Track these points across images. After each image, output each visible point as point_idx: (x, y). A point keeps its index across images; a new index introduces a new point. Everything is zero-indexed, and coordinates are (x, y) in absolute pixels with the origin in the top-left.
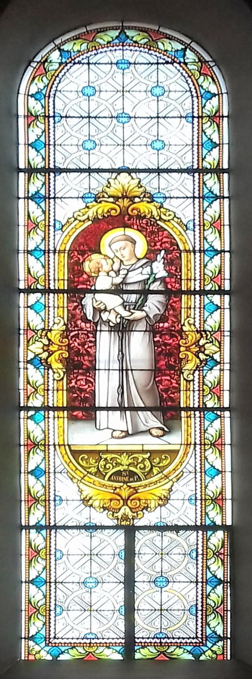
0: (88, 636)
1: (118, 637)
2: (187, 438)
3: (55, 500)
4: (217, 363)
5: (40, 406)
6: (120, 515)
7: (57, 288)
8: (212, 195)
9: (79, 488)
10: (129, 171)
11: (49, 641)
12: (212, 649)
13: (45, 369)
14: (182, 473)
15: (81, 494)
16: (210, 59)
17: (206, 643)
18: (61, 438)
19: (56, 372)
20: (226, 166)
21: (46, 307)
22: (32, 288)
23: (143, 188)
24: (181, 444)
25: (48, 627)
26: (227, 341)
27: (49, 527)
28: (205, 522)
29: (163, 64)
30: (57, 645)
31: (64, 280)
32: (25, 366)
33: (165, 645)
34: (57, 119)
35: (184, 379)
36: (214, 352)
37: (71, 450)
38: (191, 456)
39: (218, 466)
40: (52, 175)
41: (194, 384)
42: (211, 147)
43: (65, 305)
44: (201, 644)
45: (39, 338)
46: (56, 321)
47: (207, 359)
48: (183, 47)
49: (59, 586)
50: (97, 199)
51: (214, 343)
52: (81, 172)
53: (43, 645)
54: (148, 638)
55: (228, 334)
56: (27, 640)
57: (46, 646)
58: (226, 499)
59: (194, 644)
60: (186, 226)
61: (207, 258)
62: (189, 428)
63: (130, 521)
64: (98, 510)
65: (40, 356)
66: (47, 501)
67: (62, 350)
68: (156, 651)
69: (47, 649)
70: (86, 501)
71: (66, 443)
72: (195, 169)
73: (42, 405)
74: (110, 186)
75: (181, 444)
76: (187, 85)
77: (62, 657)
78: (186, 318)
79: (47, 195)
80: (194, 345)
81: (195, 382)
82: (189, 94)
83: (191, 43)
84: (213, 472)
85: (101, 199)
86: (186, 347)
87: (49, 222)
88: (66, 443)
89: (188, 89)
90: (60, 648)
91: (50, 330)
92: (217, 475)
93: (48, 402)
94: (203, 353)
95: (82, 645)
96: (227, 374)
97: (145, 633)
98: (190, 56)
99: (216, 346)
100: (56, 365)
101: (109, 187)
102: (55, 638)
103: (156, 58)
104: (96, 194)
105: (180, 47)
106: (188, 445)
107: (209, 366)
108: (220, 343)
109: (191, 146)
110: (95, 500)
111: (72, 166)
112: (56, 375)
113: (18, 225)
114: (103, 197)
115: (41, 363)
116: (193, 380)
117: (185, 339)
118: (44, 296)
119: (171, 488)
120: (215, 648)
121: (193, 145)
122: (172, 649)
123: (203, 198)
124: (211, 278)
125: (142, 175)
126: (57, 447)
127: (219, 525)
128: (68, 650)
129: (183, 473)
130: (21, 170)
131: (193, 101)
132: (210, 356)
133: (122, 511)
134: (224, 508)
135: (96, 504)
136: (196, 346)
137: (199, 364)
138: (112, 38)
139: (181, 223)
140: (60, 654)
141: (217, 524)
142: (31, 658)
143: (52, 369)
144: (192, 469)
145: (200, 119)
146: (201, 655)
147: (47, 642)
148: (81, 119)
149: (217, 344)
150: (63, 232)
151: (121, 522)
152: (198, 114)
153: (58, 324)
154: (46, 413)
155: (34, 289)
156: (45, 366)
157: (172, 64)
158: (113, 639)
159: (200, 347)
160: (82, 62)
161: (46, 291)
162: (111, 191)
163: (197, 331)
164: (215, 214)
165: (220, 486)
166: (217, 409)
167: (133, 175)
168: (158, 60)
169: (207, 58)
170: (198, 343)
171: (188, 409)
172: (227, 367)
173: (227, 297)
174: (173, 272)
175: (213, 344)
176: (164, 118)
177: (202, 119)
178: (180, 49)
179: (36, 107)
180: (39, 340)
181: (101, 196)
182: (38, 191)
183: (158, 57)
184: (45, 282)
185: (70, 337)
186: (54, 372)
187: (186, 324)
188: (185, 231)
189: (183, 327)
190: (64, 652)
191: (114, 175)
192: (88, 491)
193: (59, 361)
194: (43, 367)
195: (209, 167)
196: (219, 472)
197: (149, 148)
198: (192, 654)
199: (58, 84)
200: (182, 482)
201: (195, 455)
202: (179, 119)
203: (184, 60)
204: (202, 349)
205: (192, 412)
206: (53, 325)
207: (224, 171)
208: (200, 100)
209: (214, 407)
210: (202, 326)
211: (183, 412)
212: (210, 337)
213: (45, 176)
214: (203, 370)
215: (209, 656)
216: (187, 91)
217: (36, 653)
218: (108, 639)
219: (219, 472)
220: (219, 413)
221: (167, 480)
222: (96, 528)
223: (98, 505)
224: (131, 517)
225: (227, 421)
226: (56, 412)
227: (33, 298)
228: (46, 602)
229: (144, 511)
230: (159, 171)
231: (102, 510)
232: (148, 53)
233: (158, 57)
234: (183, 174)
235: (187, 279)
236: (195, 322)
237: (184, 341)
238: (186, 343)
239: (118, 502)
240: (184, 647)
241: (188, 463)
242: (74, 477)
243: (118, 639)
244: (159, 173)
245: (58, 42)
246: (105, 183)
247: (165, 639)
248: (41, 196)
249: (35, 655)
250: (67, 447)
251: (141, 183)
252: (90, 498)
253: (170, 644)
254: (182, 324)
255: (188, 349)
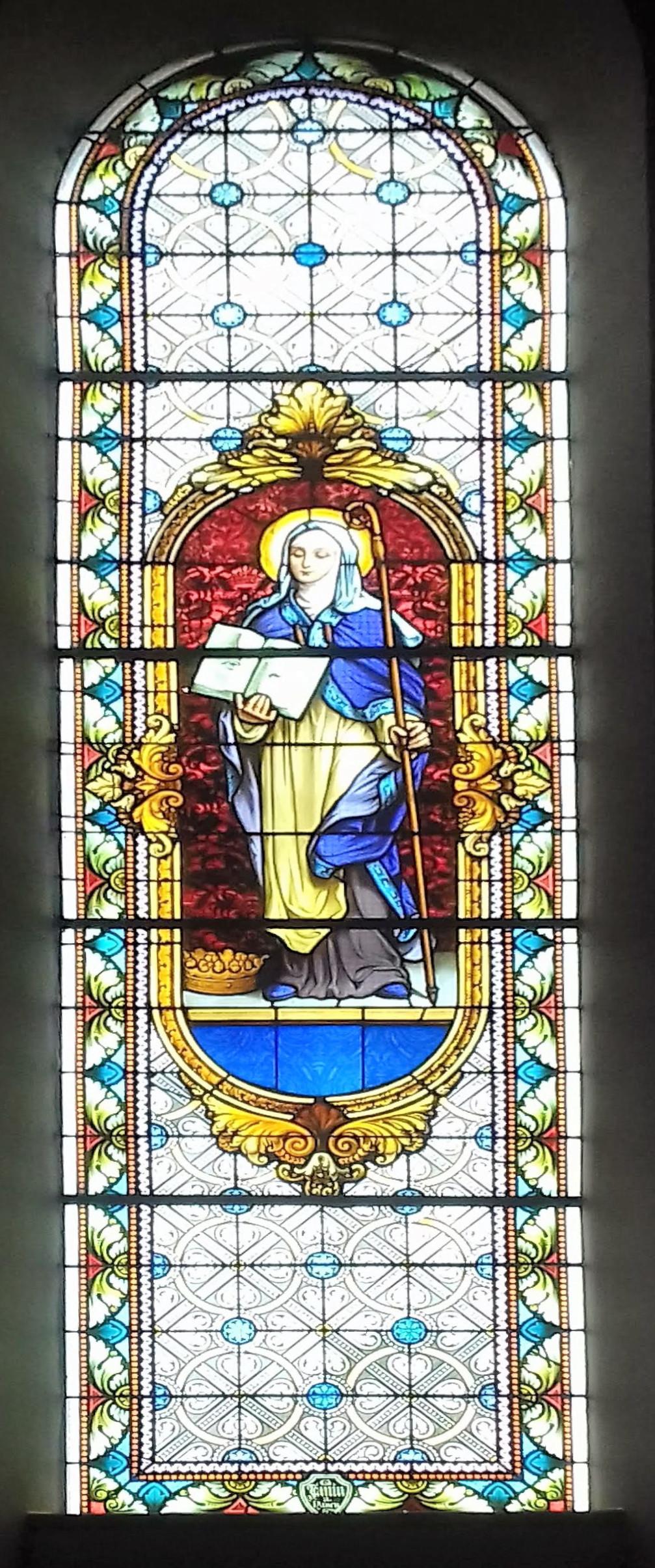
0: (233, 1457)
1: (309, 1459)
2: (472, 992)
3: (149, 1135)
4: (546, 817)
5: (116, 917)
6: (308, 1170)
7: (148, 645)
8: (525, 435)
9: (208, 1111)
10: (324, 377)
11: (138, 1468)
12: (537, 1486)
13: (126, 833)
14: (458, 1075)
15: (214, 1122)
16: (523, 123)
17: (522, 1473)
18: (166, 992)
19: (154, 839)
20: (558, 364)
21: (127, 691)
22: (89, 645)
23: (357, 417)
24: (457, 1007)
25: (136, 1435)
26: (567, 767)
27: (135, 1199)
28: (516, 1191)
29: (406, 130)
30: (159, 1477)
31: (165, 627)
32: (80, 826)
33: (248, 1479)
34: (158, 1270)
35: (468, 854)
36: (536, 791)
37: (188, 1021)
38: (482, 1035)
39: (552, 1316)
40: (138, 386)
41: (490, 867)
42: (521, 322)
43: (174, 687)
44: (509, 1477)
45: (112, 765)
46: (152, 721)
47: (521, 807)
48: (454, 92)
49: (162, 1339)
50: (247, 442)
51: (536, 770)
52: (377, 382)
53: (124, 1477)
54: (381, 1462)
55: (64, 748)
56: (85, 1467)
57: (131, 1480)
58: (77, 1137)
59: (493, 1477)
60: (462, 504)
61: (512, 577)
62: (477, 968)
63: (332, 1187)
64: (254, 1159)
65: (116, 805)
66: (513, 1136)
67: (167, 789)
68: (400, 1494)
69: (134, 1487)
70: (223, 1139)
71: (178, 1004)
72: (492, 657)
73: (120, 914)
74: (279, 412)
75: (457, 1007)
76: (460, 177)
77: (172, 1507)
78: (466, 714)
79: (127, 433)
80: (489, 777)
81: (492, 862)
82: (467, 198)
83: (472, 84)
84: (535, 1072)
85: (256, 442)
86: (470, 781)
87: (130, 493)
88: (178, 1004)
89: (464, 188)
90: (167, 1484)
91: (139, 746)
92: (546, 1078)
93: (136, 908)
94: (512, 794)
95: (391, 1476)
96: (569, 842)
97: (372, 1450)
98: (470, 115)
99: (540, 777)
100: (153, 823)
101: (275, 415)
102: (152, 1459)
103: (386, 116)
104: (243, 429)
105: (446, 91)
106: (476, 1008)
107: (528, 822)
108: (550, 771)
109: (475, 317)
110: (247, 1137)
111: (187, 367)
112: (154, 848)
113: (578, 943)
114: (262, 436)
115: (118, 819)
116: (489, 857)
117: (465, 763)
118: (120, 666)
119: (434, 1109)
120: (544, 1485)
121: (479, 313)
122: (263, 1488)
123: (506, 561)
124: (522, 621)
125: (353, 388)
126: (156, 1013)
127: (550, 1196)
128: (185, 1488)
129: (463, 1073)
130: (66, 377)
131: (478, 215)
132: (527, 800)
133: (314, 1161)
134: (557, 900)
135: (251, 1145)
136: (494, 778)
137: (501, 820)
138: (285, 68)
139: (449, 497)
140: (166, 1499)
141: (546, 1193)
142: (98, 1508)
143: (144, 833)
144: (485, 1066)
145: (497, 257)
146: (509, 1503)
147: (135, 1471)
148: (209, 257)
149: (543, 772)
150: (166, 516)
151: (312, 1188)
152: (492, 244)
153: (157, 729)
154: (131, 934)
155: (532, 646)
156: (126, 826)
157: (430, 132)
158: (467, 1463)
159: (503, 781)
160: (214, 127)
161: (126, 655)
162: (282, 424)
163: (494, 743)
164: (533, 477)
165: (544, 720)
166: (545, 923)
167: (336, 387)
168: (391, 122)
169: (516, 120)
170: (136, 798)
171: (474, 923)
172: (570, 824)
173: (565, 663)
174: (430, 606)
175: (534, 774)
176: (243, 254)
177: (501, 257)
178: (446, 95)
179: (101, 228)
180: (113, 768)
181: (257, 435)
182: (105, 425)
183: (391, 115)
184: (120, 631)
185: (184, 760)
186: (149, 841)
187: (467, 728)
188: (459, 516)
189: (459, 735)
190: (177, 1493)
191: (289, 386)
192: (227, 1116)
193: (160, 815)
194: (122, 829)
195: (518, 368)
196: (550, 1072)
197: (208, 321)
198: (487, 1499)
199: (155, 176)
200: (458, 1096)
201: (492, 1031)
202: (446, 257)
203: (457, 121)
204: (507, 785)
205: (485, 931)
206: (146, 732)
207: (554, 376)
208: (495, 214)
209: (541, 917)
210: (505, 734)
211: (462, 932)
212: (527, 758)
213: (122, 389)
214: (511, 832)
215: (530, 1504)
216: (461, 192)
217: (108, 1498)
218: (283, 1463)
219: (550, 1072)
220: (548, 933)
221: (425, 1092)
222: (250, 1200)
223: (254, 1148)
224: (334, 1179)
225: (571, 954)
226: (154, 932)
227: (94, 671)
228: (131, 1379)
229: (368, 1164)
230: (398, 376)
231: (264, 1160)
232: (368, 105)
233: (391, 115)
234: (456, 384)
235: (472, 880)
236: (488, 722)
237: (463, 768)
238: (467, 772)
239: (302, 1141)
240: (469, 1484)
241: (473, 1051)
242: (195, 1083)
243: (480, 1463)
244: (229, 382)
245: (150, 82)
246: (266, 404)
247: (423, 1465)
248: (113, 435)
249: (105, 1501)
250: (179, 1013)
251: (354, 407)
252: (235, 1133)
253: (260, 1477)
254: (457, 727)
255: (473, 785)
